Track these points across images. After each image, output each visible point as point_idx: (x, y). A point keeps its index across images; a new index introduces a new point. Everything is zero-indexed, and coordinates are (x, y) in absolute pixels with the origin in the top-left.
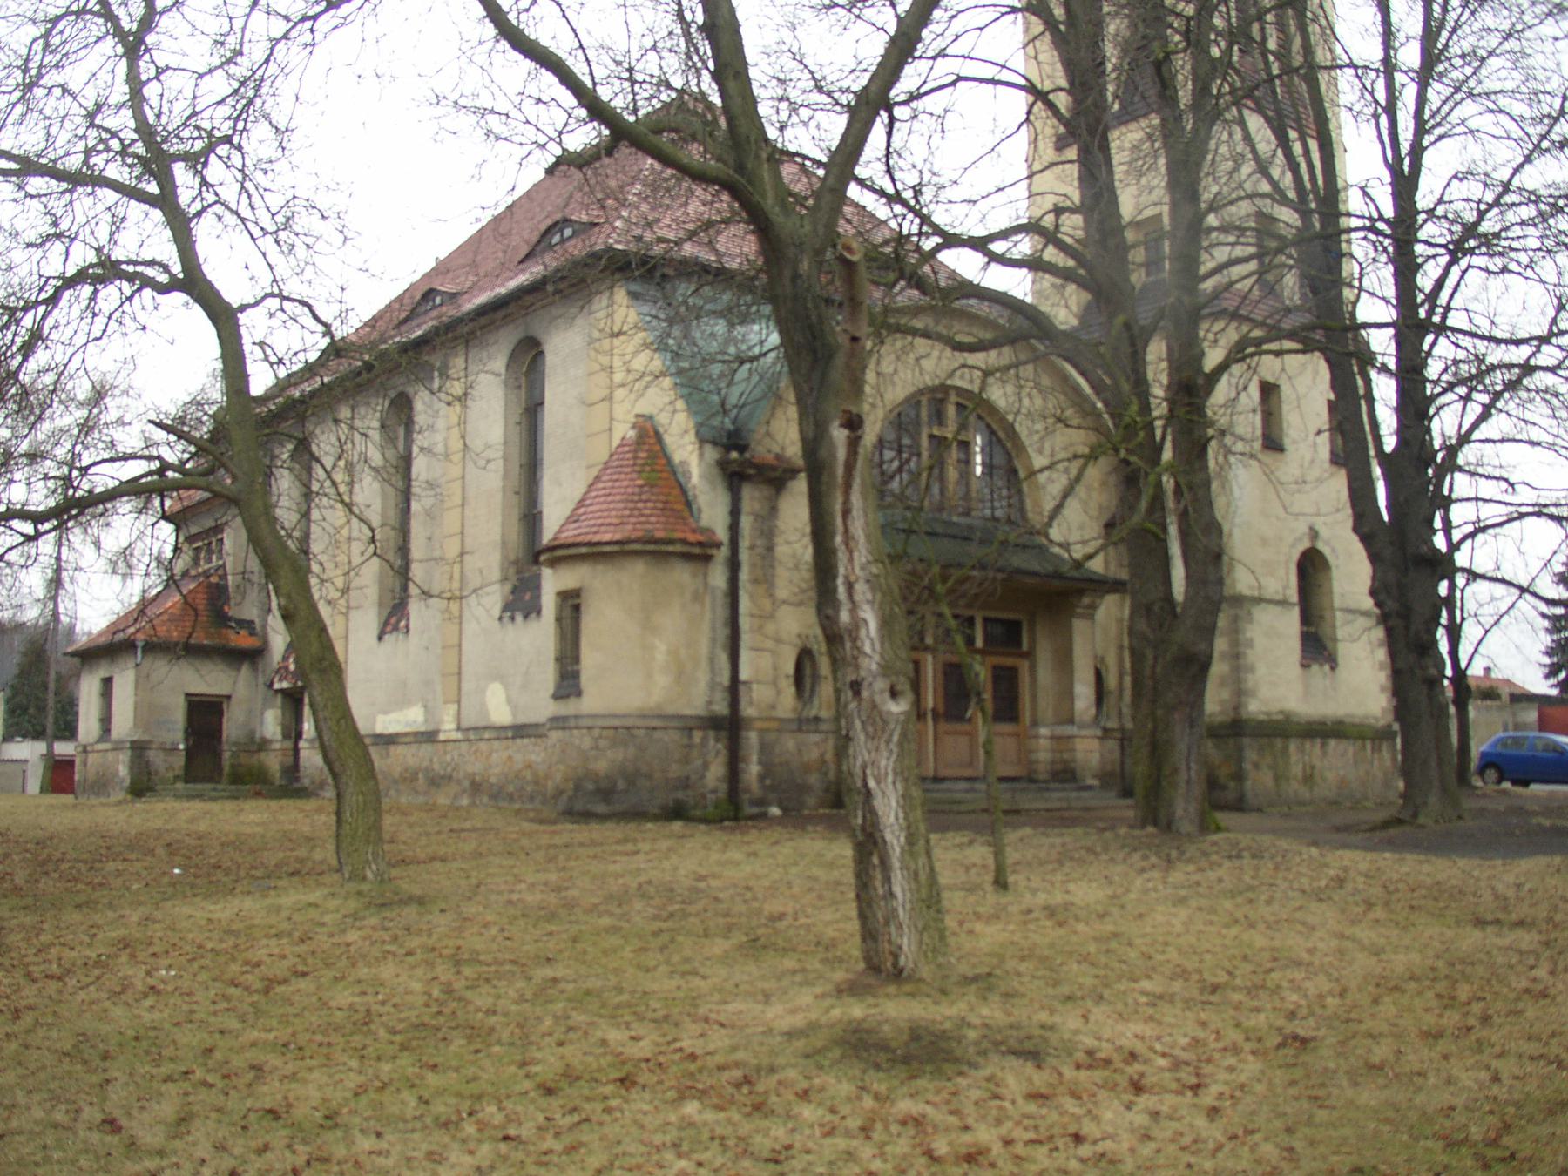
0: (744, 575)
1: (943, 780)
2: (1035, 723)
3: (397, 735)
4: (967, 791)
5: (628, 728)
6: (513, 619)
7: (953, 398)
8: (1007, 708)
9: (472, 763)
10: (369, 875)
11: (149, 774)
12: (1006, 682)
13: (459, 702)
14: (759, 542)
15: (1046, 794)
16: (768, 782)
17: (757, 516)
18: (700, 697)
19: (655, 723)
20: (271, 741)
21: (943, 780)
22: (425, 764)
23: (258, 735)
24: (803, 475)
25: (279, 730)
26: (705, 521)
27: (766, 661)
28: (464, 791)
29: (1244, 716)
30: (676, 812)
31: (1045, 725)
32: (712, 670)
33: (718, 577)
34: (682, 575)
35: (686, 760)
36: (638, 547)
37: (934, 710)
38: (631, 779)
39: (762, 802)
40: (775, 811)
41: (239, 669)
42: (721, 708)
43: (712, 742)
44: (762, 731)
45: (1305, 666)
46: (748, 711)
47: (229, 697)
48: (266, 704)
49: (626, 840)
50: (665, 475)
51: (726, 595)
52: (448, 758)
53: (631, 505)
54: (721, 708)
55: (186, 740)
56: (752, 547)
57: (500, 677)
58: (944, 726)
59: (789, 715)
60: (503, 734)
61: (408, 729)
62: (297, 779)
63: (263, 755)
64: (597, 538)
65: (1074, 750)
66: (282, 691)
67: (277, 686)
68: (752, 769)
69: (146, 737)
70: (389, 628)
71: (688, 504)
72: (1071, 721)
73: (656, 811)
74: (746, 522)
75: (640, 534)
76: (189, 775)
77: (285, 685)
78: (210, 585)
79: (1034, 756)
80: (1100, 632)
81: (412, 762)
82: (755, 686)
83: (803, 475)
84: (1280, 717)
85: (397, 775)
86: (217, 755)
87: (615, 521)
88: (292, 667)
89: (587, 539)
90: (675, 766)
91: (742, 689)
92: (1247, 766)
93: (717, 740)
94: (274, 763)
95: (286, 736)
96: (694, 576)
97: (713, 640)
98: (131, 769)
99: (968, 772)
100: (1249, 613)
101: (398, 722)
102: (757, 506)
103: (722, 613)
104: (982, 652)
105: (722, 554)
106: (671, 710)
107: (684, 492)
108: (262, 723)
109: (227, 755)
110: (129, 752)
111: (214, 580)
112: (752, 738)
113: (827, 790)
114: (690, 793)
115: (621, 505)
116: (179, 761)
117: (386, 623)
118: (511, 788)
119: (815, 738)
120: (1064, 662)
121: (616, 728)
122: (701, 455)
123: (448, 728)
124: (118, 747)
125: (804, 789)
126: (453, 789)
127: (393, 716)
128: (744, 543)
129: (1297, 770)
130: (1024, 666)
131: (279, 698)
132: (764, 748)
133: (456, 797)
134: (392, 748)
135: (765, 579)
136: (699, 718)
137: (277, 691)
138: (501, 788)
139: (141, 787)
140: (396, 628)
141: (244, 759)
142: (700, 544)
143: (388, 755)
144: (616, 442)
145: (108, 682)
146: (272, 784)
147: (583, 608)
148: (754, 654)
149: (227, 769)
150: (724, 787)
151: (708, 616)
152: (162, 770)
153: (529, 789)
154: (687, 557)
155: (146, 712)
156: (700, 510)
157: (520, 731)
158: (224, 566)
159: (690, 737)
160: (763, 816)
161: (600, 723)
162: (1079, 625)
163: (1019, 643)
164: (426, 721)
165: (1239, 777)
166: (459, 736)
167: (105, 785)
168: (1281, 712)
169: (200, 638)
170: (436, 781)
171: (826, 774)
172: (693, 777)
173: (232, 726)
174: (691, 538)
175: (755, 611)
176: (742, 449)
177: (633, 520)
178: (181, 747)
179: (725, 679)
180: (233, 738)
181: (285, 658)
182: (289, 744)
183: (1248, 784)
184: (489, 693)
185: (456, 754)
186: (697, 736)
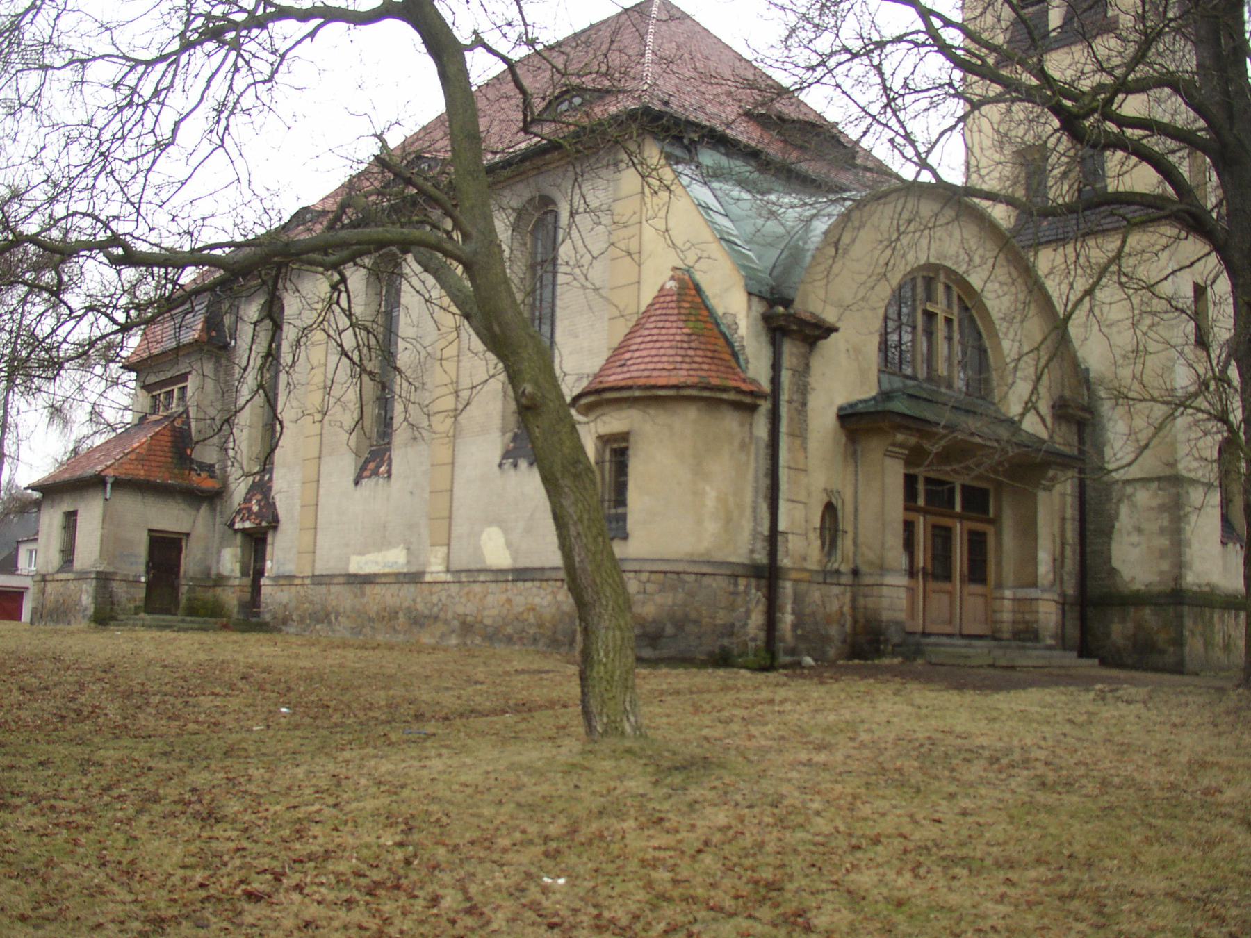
0: (784, 428)
1: (930, 635)
2: (1000, 586)
3: (375, 575)
4: (966, 646)
5: (678, 573)
6: (515, 465)
7: (942, 278)
8: (977, 572)
9: (464, 606)
10: (628, 729)
11: (112, 603)
12: (977, 543)
13: (449, 545)
14: (795, 397)
15: (1029, 652)
16: (799, 632)
17: (795, 372)
18: (743, 546)
19: (705, 569)
20: (228, 578)
21: (930, 635)
22: (406, 604)
23: (214, 571)
24: (570, 389)
25: (237, 567)
26: (751, 374)
27: (799, 512)
28: (453, 631)
29: (1184, 587)
30: (723, 660)
31: (1009, 588)
32: (755, 519)
33: (761, 429)
34: (731, 422)
35: (732, 608)
36: (694, 393)
37: (924, 568)
38: (680, 624)
39: (792, 651)
40: (808, 660)
41: (198, 510)
42: (762, 558)
43: (753, 591)
44: (796, 581)
45: (1224, 544)
46: (785, 561)
47: (188, 535)
48: (223, 543)
49: (725, 689)
50: (709, 326)
51: (767, 446)
52: (435, 599)
53: (682, 352)
54: (762, 558)
55: (147, 572)
56: (790, 402)
57: (500, 523)
58: (932, 585)
59: (815, 567)
60: (501, 578)
61: (387, 570)
62: (257, 615)
63: (219, 590)
64: (652, 382)
65: (1037, 612)
66: (243, 531)
67: (238, 526)
68: (787, 618)
69: (111, 569)
70: (367, 473)
71: (735, 355)
72: (1034, 585)
73: (702, 657)
74: (786, 376)
75: (695, 380)
76: (150, 605)
77: (247, 525)
78: (174, 430)
79: (998, 616)
80: (1054, 504)
81: (390, 601)
82: (790, 537)
83: (570, 389)
84: (1207, 589)
85: (372, 614)
86: (175, 589)
87: (667, 366)
88: (255, 508)
89: (641, 382)
90: (721, 613)
91: (780, 538)
92: (1186, 633)
93: (758, 589)
94: (231, 598)
95: (244, 573)
96: (742, 425)
97: (756, 490)
98: (95, 598)
99: (948, 629)
100: (1188, 493)
101: (377, 563)
102: (795, 361)
103: (764, 464)
104: (961, 517)
105: (765, 406)
106: (719, 556)
107: (729, 343)
108: (218, 562)
109: (184, 589)
110: (94, 583)
111: (178, 424)
112: (787, 587)
113: (844, 642)
114: (734, 640)
115: (672, 352)
116: (142, 593)
117: (363, 468)
118: (509, 630)
119: (836, 590)
120: (1028, 531)
121: (665, 573)
122: (749, 307)
123: (435, 567)
124: (82, 576)
125: (826, 639)
126: (440, 628)
127: (370, 557)
128: (784, 397)
129: (1218, 638)
130: (990, 530)
131: (239, 539)
132: (798, 599)
133: (443, 636)
134: (368, 588)
135: (800, 434)
136: (743, 565)
137: (239, 530)
138: (498, 630)
139: (104, 617)
140: (375, 473)
141: (200, 593)
142: (751, 393)
143: (363, 594)
144: (647, 297)
145: (71, 517)
146: (229, 617)
147: (631, 452)
148: (791, 505)
149: (183, 602)
150: (762, 635)
151: (752, 465)
152: (124, 600)
153: (532, 632)
154: (737, 406)
155: (111, 544)
156: (747, 362)
157: (521, 574)
158: (186, 412)
159: (736, 584)
160: (798, 665)
161: (648, 567)
162: (1042, 495)
163: (986, 511)
164: (408, 562)
165: (1179, 642)
166: (449, 577)
167: (66, 613)
168: (1208, 584)
169: (159, 476)
170: (418, 621)
171: (843, 626)
172: (738, 624)
173: (190, 562)
174: (744, 387)
175: (792, 465)
176: (787, 303)
177: (685, 366)
178: (143, 579)
179: (765, 529)
180: (191, 574)
181: (247, 500)
182: (247, 581)
183: (1187, 649)
184: (484, 536)
185: (444, 595)
186: (742, 582)
